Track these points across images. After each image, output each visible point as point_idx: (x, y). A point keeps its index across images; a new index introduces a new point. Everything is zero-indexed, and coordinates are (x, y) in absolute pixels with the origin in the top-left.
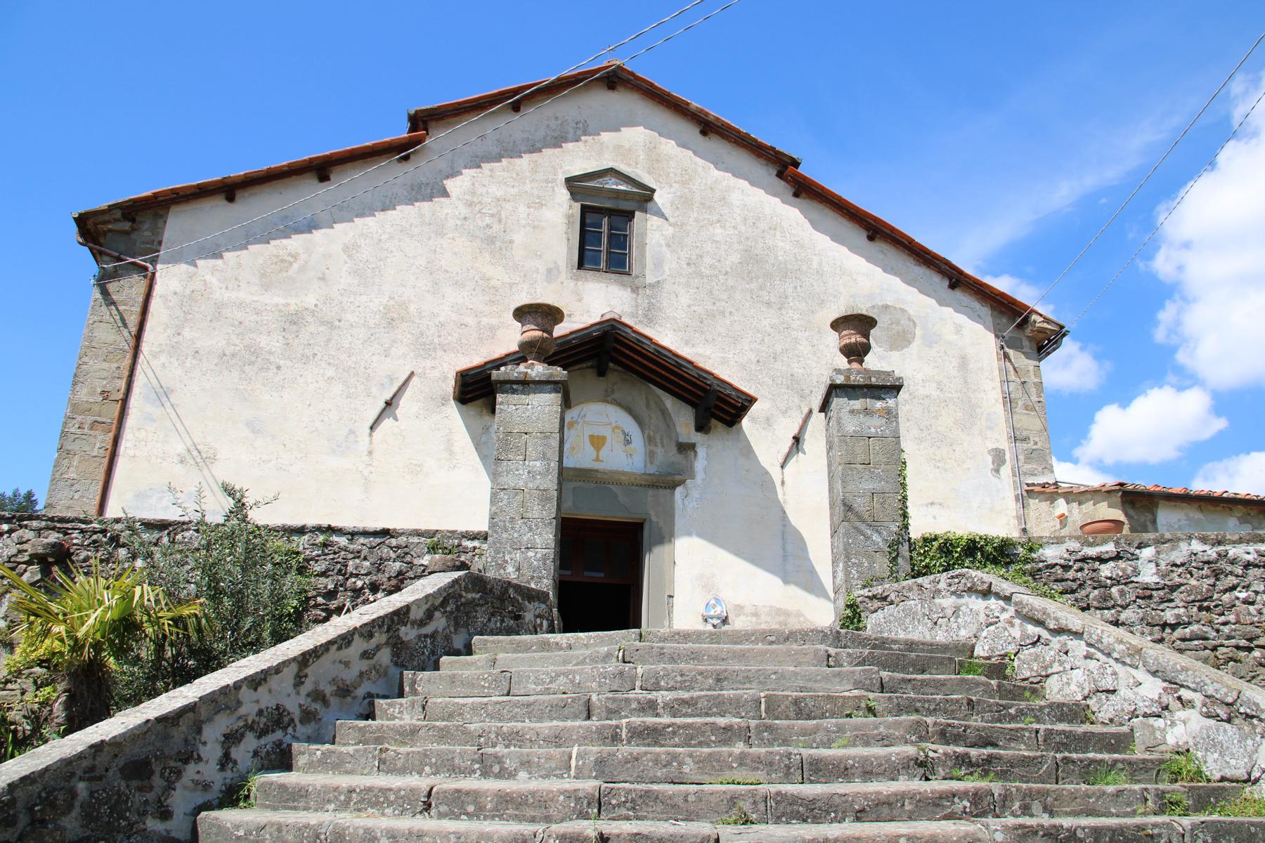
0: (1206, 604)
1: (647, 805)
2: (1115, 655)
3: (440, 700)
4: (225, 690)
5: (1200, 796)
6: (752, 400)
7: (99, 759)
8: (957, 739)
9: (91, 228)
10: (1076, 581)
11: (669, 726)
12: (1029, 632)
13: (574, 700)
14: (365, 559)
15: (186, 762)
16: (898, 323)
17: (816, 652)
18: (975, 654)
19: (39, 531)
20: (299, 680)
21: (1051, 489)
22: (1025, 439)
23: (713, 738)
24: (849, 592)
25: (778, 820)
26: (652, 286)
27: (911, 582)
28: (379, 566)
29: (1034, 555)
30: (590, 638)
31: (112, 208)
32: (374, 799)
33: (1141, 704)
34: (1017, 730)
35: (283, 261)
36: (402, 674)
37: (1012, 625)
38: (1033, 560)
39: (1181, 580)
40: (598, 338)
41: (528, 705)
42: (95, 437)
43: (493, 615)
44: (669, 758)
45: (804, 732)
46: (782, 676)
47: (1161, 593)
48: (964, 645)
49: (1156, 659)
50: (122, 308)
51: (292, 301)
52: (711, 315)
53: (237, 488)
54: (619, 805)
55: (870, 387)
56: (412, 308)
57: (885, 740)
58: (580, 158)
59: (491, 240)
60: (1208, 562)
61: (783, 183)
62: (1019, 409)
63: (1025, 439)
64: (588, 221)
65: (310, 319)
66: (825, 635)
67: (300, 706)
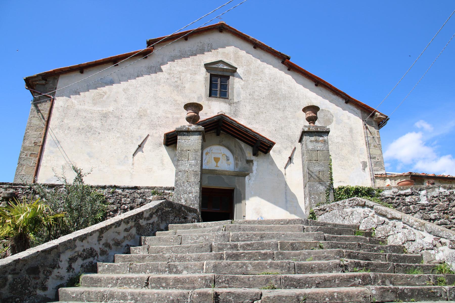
0: (446, 211)
1: (233, 282)
2: (414, 227)
3: (154, 246)
4: (69, 241)
5: (450, 278)
6: (273, 144)
7: (17, 266)
8: (355, 257)
9: (31, 83)
10: (396, 202)
11: (242, 253)
12: (381, 220)
13: (205, 245)
14: (128, 198)
15: (54, 268)
16: (327, 116)
17: (299, 227)
18: (360, 229)
19: (6, 189)
20: (100, 239)
21: (385, 176)
22: (374, 158)
23: (260, 258)
24: (311, 208)
25: (285, 287)
26: (236, 103)
27: (334, 203)
28: (133, 201)
29: (380, 194)
30: (212, 224)
31: (38, 76)
32: (126, 282)
33: (425, 245)
34: (378, 255)
35: (101, 95)
36: (141, 238)
37: (374, 217)
38: (380, 196)
39: (436, 203)
40: (216, 122)
41: (188, 247)
42: (32, 159)
43: (176, 217)
44: (242, 264)
45: (295, 255)
46: (286, 236)
47: (429, 207)
48: (355, 225)
49: (431, 227)
50: (42, 112)
51: (104, 109)
52: (258, 113)
53: (78, 169)
54: (222, 282)
55: (318, 132)
56: (148, 111)
57: (326, 258)
58: (210, 57)
59: (177, 87)
60: (446, 196)
61: (284, 65)
62: (372, 147)
63: (374, 158)
64: (213, 80)
65: (111, 116)
66: (302, 221)
67: (100, 248)
